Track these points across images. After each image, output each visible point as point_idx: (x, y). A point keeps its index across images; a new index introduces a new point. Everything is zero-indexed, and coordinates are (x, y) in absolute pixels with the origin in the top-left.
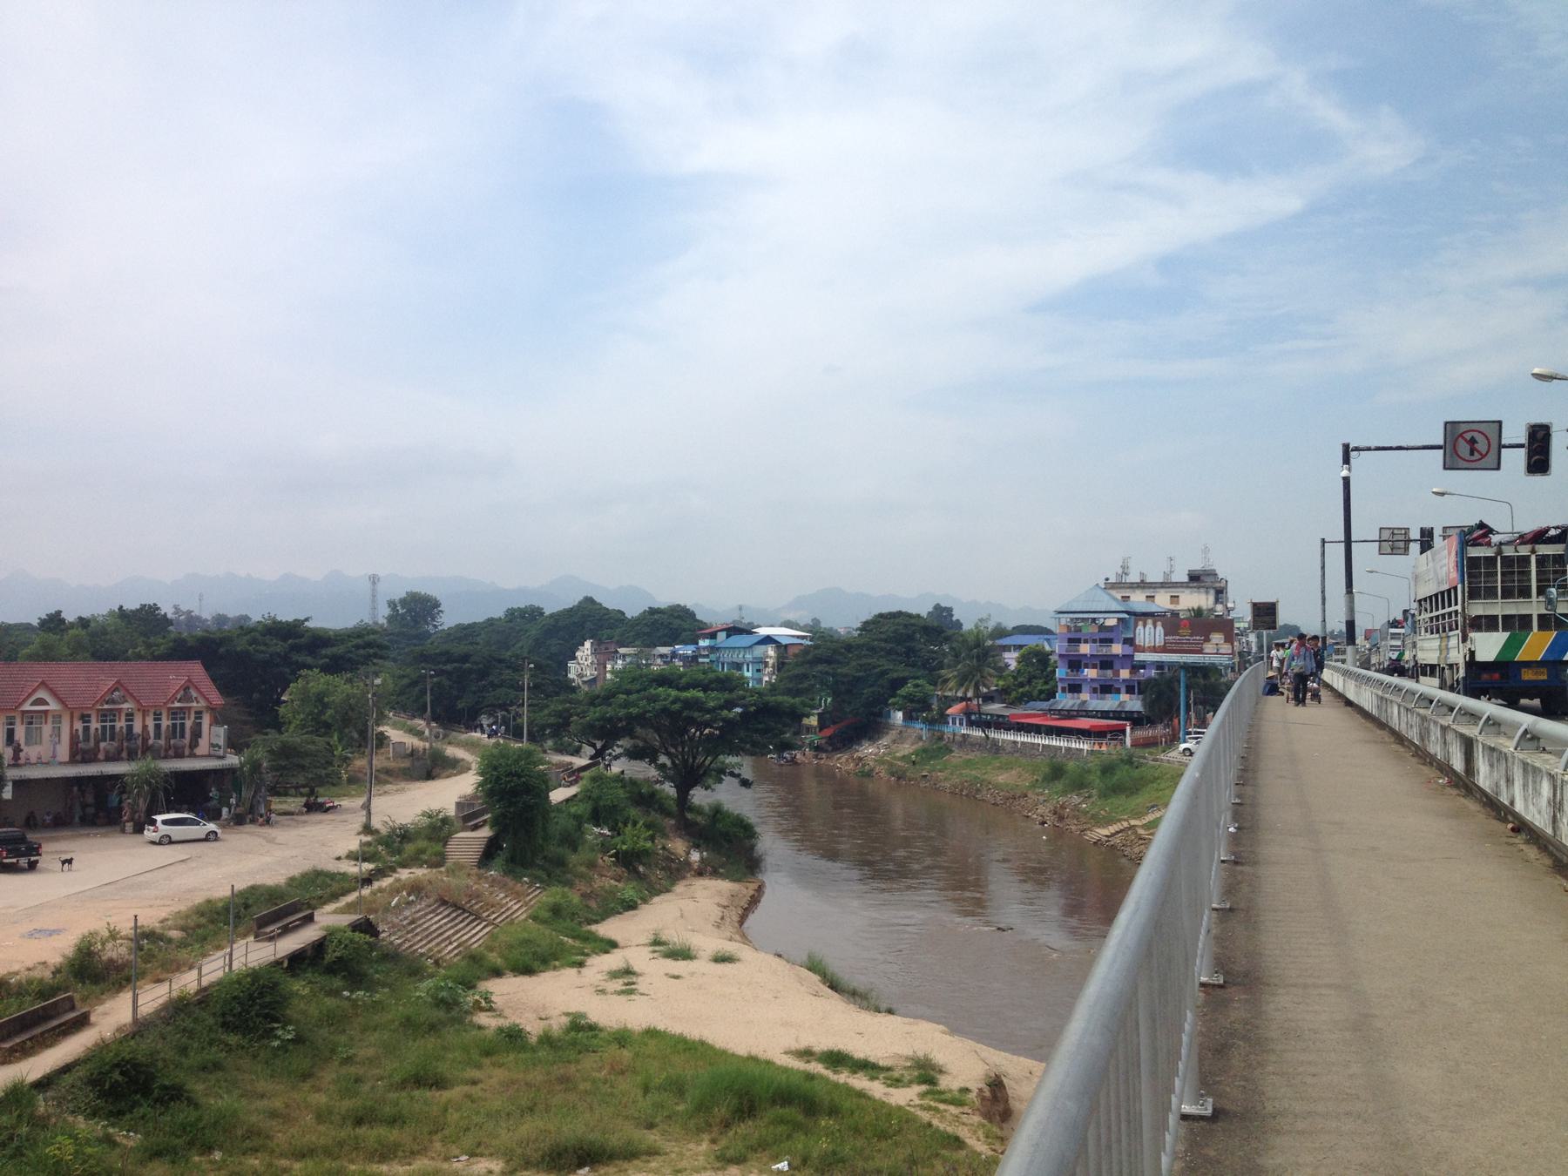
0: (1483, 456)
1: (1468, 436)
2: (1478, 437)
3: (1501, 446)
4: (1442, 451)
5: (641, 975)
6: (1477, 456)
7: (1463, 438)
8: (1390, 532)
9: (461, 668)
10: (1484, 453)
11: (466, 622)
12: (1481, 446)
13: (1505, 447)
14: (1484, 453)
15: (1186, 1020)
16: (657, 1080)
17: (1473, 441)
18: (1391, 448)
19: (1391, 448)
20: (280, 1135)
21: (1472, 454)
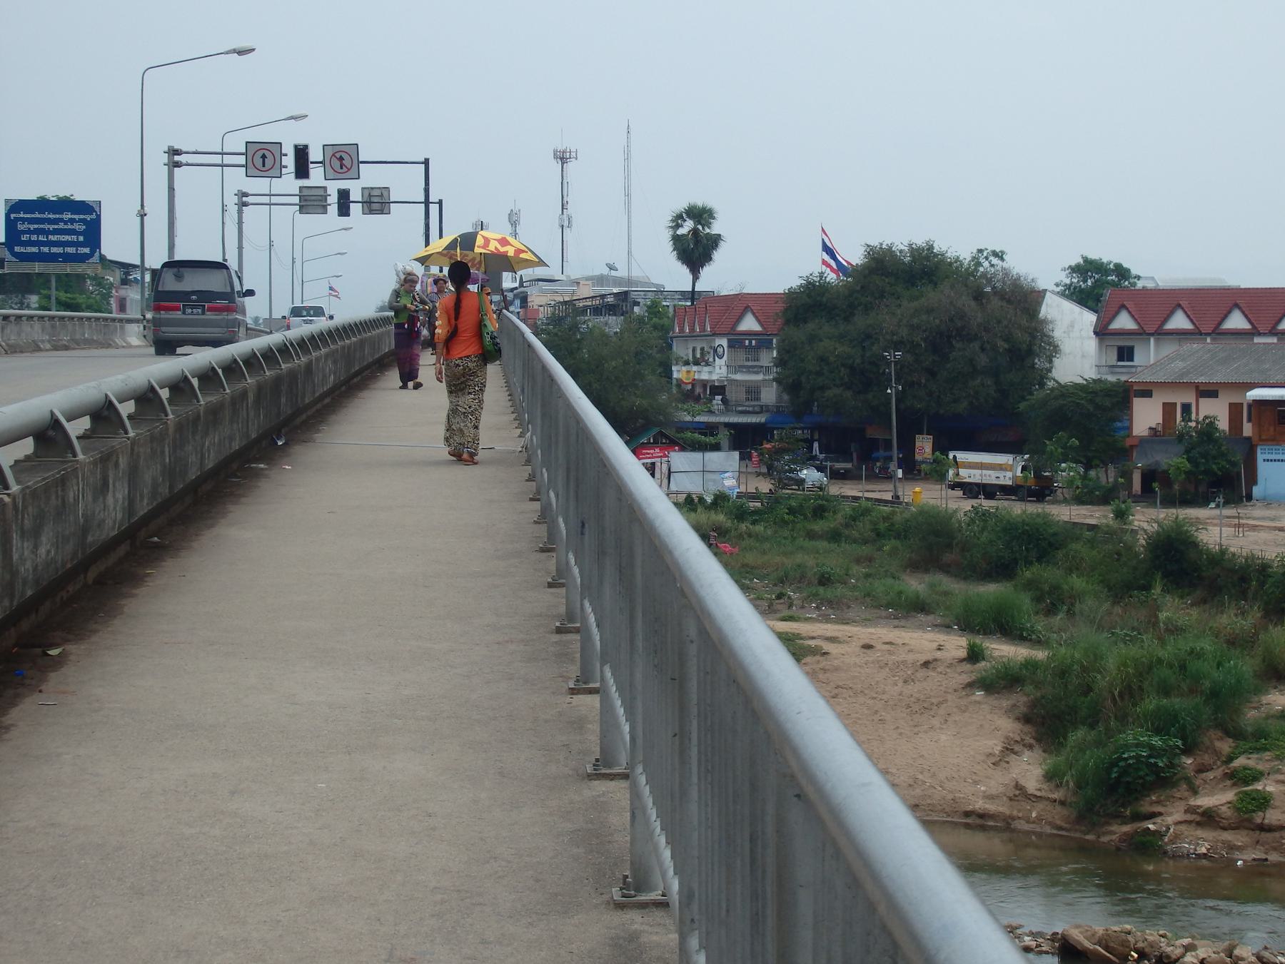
0: (349, 170)
1: (338, 155)
2: (344, 156)
3: (246, 166)
4: (360, 160)
5: (970, 685)
6: (345, 169)
7: (335, 157)
8: (384, 212)
9: (147, 299)
10: (349, 167)
11: (78, 198)
12: (347, 162)
13: (243, 166)
14: (349, 167)
15: (836, 476)
16: (944, 587)
17: (341, 159)
18: (407, 163)
19: (407, 163)
20: (666, 319)
21: (342, 168)
